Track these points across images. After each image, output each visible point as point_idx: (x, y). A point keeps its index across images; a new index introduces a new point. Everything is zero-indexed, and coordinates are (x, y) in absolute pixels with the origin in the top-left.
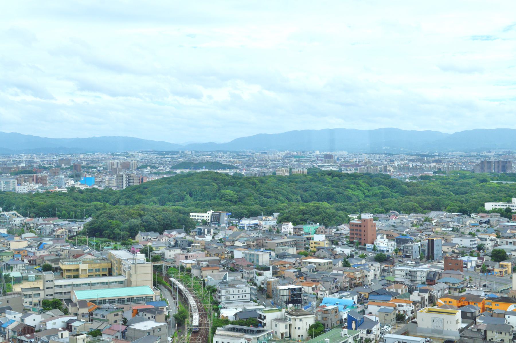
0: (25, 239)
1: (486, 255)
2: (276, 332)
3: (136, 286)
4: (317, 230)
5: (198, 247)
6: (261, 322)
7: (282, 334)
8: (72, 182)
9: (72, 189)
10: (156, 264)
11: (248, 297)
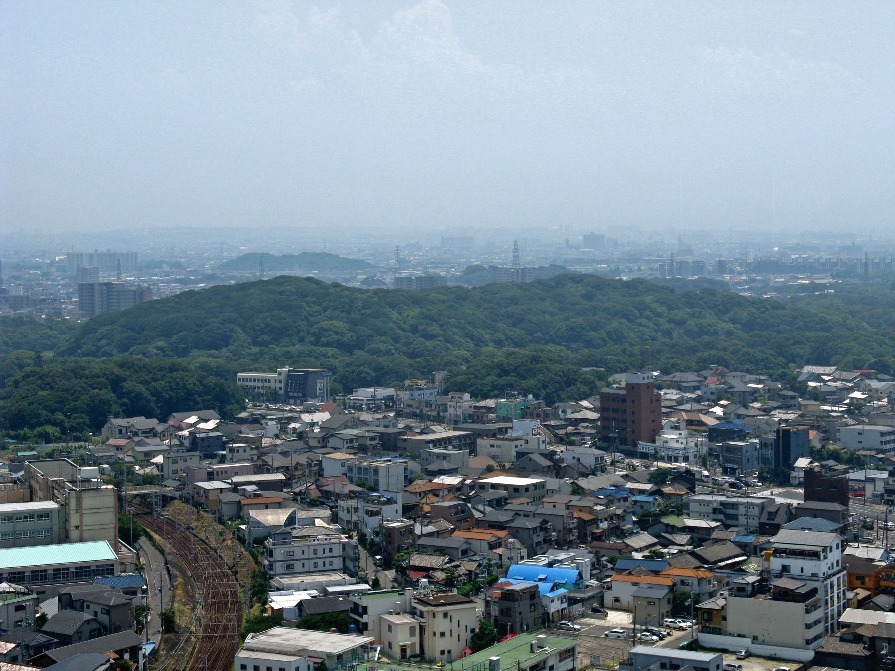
2: (390, 644)
3: (81, 540)
4: (528, 410)
5: (241, 451)
6: (356, 622)
7: (403, 649)
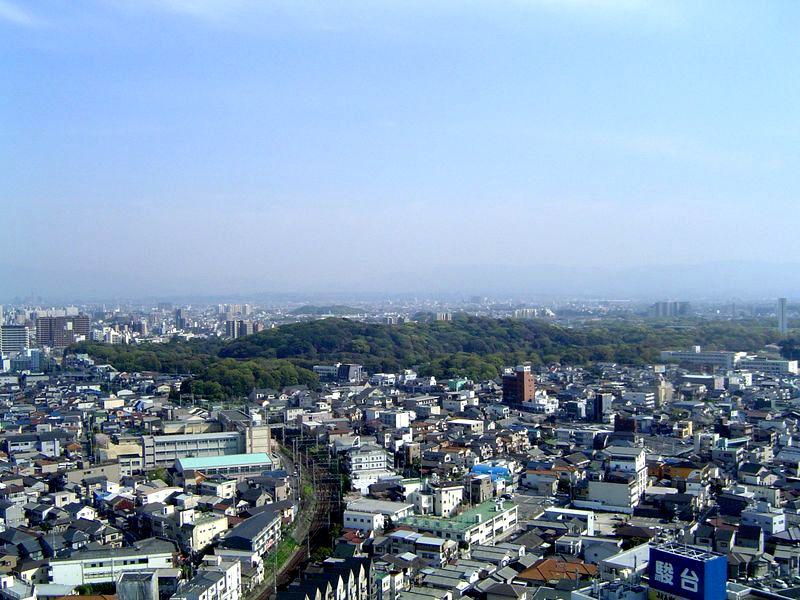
0: (120, 397)
1: (663, 413)
8: (175, 331)
9: (175, 338)
10: (274, 426)
11: (384, 465)
